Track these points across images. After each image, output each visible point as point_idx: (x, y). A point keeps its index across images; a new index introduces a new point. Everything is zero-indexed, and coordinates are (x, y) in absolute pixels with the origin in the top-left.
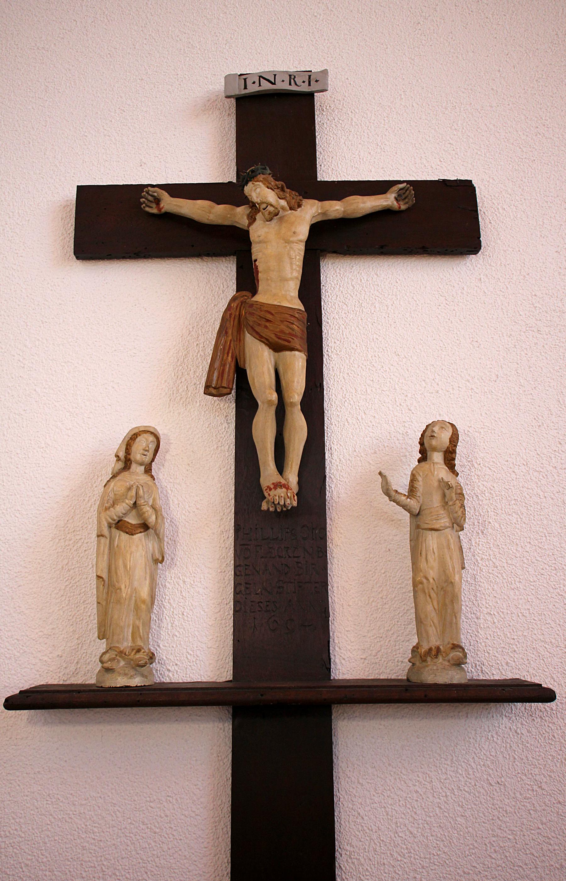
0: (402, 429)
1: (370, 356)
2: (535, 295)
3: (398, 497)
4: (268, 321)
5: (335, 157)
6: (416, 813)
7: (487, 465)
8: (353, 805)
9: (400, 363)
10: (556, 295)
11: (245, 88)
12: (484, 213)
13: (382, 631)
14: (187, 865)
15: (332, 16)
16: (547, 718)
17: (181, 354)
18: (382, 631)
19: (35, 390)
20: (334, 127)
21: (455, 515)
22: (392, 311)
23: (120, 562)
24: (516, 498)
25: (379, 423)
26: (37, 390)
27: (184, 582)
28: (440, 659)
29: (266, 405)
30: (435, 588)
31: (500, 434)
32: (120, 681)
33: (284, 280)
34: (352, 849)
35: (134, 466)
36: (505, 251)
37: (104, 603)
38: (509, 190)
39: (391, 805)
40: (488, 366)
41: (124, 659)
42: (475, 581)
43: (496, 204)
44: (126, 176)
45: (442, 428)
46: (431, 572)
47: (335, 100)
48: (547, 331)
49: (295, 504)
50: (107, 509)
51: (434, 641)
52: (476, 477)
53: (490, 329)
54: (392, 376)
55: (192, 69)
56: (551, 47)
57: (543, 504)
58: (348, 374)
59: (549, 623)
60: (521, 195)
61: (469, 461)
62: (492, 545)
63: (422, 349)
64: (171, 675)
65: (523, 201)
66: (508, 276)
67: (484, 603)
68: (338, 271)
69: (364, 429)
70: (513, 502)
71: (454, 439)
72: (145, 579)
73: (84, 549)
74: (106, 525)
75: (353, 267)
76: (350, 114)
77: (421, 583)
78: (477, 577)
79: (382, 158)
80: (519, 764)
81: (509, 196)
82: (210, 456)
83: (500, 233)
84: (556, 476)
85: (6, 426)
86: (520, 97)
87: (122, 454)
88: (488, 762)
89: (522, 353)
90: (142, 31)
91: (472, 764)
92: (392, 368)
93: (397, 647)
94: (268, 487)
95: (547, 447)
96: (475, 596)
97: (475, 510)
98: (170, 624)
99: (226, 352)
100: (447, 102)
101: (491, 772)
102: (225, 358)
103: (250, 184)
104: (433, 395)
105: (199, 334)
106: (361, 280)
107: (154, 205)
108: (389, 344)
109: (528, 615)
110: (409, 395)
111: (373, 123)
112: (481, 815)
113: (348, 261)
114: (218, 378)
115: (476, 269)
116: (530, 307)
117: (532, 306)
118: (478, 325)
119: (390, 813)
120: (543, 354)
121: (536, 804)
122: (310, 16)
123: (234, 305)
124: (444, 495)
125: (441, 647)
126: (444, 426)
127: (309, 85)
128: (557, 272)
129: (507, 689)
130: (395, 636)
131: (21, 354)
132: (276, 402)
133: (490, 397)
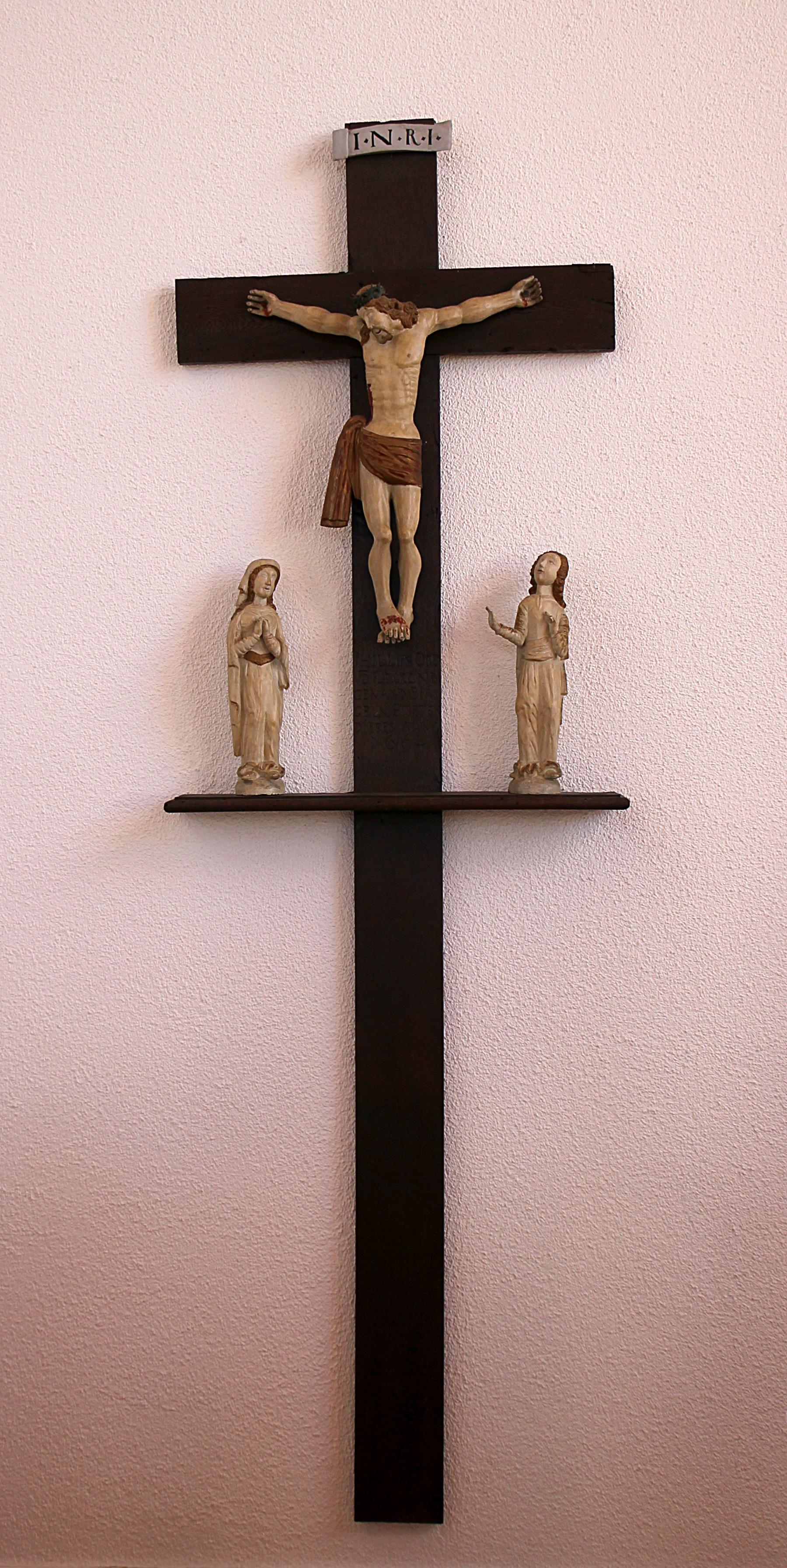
0: (521, 551)
1: (491, 473)
2: (674, 398)
3: (502, 631)
4: (382, 455)
5: (460, 225)
6: (514, 902)
7: (604, 589)
8: (460, 895)
9: (523, 480)
10: (697, 397)
11: (357, 148)
12: (627, 296)
13: (491, 750)
14: (318, 939)
15: (462, 17)
16: (639, 826)
17: (294, 473)
18: (491, 750)
19: (150, 514)
20: (461, 183)
21: (556, 647)
22: (517, 420)
23: (251, 690)
24: (631, 623)
25: (497, 546)
26: (152, 513)
27: (307, 704)
28: (535, 774)
29: (381, 543)
30: (535, 713)
31: (620, 557)
32: (259, 791)
33: (396, 408)
34: (458, 929)
35: (257, 598)
36: (646, 344)
37: (239, 725)
38: (659, 265)
39: (494, 895)
40: (615, 483)
41: (259, 773)
42: (583, 703)
43: (642, 284)
44: (225, 255)
45: (550, 562)
46: (532, 698)
47: (463, 145)
48: (682, 440)
49: (408, 637)
50: (237, 641)
51: (532, 759)
52: (592, 602)
53: (621, 440)
54: (514, 495)
55: (293, 103)
56: (730, 57)
57: (657, 629)
58: (467, 493)
59: (650, 743)
60: (672, 270)
61: (587, 586)
62: (602, 670)
63: (547, 464)
64: (298, 787)
65: (673, 278)
66: (646, 375)
67: (590, 725)
68: (460, 372)
69: (482, 552)
70: (627, 627)
71: (563, 572)
72: (274, 704)
73: (212, 673)
74: (237, 656)
75: (476, 367)
76: (480, 164)
77: (523, 708)
78: (585, 700)
79: (514, 225)
80: (609, 864)
81: (657, 272)
82: (327, 582)
83: (643, 322)
84: (673, 600)
85: (125, 551)
86: (684, 133)
87: (245, 588)
88: (582, 863)
89: (653, 466)
90: (232, 48)
91: (568, 864)
92: (513, 485)
93: (506, 764)
94: (384, 620)
95: (668, 570)
96: (582, 718)
97: (589, 635)
98: (295, 743)
99: (341, 482)
100: (596, 143)
101: (584, 870)
102: (340, 489)
103: (362, 308)
104: (554, 515)
105: (312, 450)
106: (485, 384)
107: (261, 308)
108: (511, 459)
109: (631, 735)
110: (530, 516)
111: (506, 177)
112: (572, 904)
113: (472, 360)
114: (334, 510)
115: (612, 367)
116: (666, 412)
117: (669, 411)
118: (608, 434)
119: (492, 902)
120: (675, 467)
121: (621, 896)
122: (434, 18)
123: (348, 432)
124: (548, 627)
125: (538, 764)
126: (552, 560)
127: (430, 143)
128: (702, 369)
129: (588, 799)
130: (504, 754)
131: (132, 474)
132: (391, 539)
133: (614, 516)
